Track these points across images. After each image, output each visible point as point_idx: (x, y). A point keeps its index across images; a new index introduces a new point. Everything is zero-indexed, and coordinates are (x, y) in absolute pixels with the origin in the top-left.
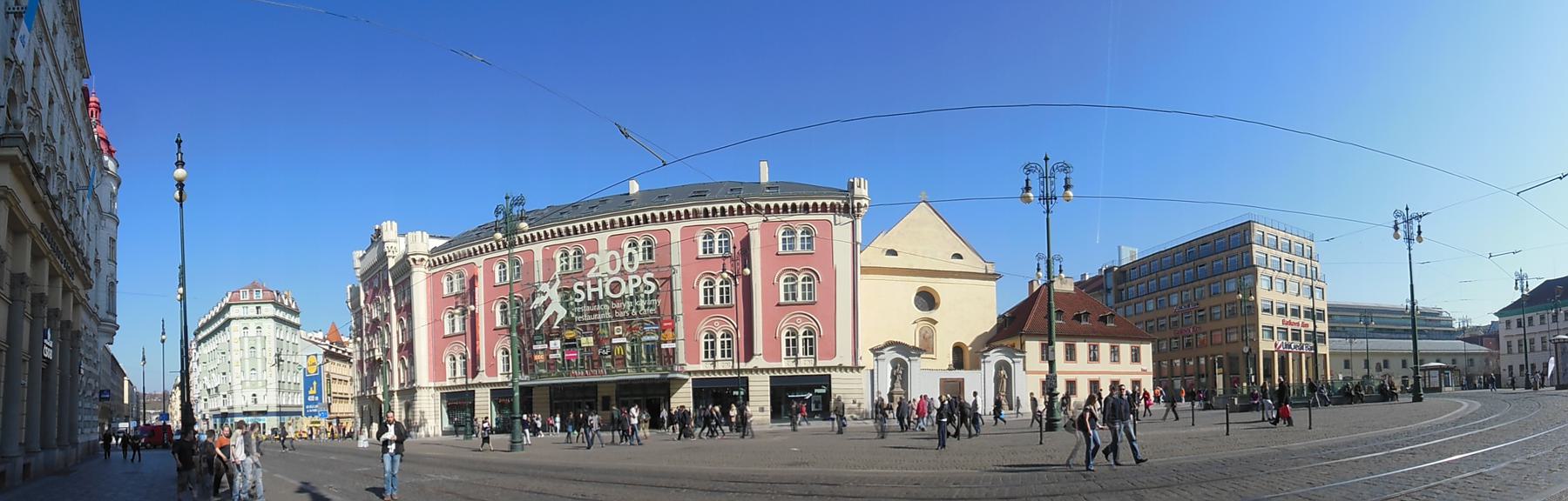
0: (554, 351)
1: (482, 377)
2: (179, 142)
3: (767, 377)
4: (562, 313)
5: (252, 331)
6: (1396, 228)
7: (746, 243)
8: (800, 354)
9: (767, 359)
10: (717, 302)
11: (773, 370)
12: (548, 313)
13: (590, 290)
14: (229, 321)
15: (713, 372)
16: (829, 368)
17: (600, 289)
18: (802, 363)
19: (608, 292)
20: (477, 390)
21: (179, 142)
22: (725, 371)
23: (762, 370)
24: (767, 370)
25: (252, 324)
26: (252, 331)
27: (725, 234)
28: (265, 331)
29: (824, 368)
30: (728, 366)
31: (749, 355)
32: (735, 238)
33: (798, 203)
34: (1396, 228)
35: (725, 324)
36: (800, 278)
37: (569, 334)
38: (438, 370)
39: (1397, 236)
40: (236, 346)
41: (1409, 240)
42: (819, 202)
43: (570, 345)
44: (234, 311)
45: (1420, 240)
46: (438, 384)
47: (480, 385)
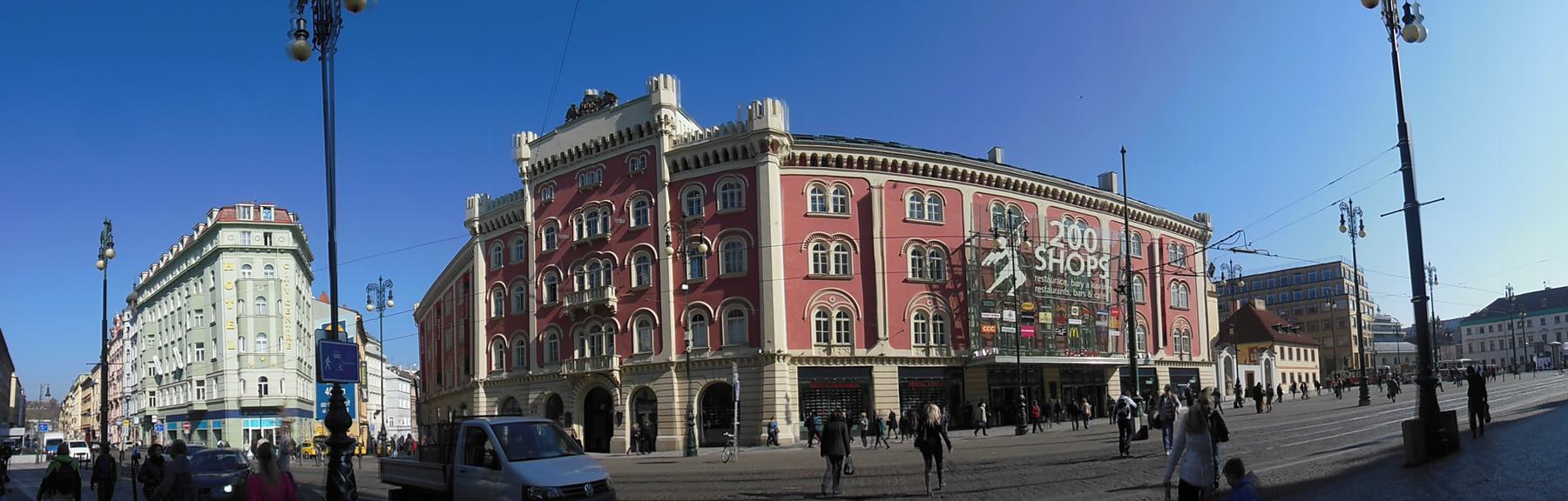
0: (1009, 324)
1: (884, 348)
2: (1123, 151)
3: (895, 367)
4: (1021, 279)
5: (258, 271)
6: (1343, 222)
7: (865, 205)
8: (834, 341)
9: (895, 345)
10: (832, 272)
11: (902, 359)
12: (1005, 274)
13: (1052, 260)
14: (217, 253)
15: (828, 360)
16: (870, 359)
17: (1061, 262)
18: (836, 352)
19: (1068, 266)
20: (877, 368)
21: (1123, 151)
22: (842, 359)
23: (889, 360)
24: (895, 360)
25: (258, 260)
26: (258, 271)
27: (841, 190)
28: (279, 272)
29: (863, 359)
30: (845, 352)
31: (871, 339)
32: (855, 193)
33: (821, 154)
34: (1343, 222)
35: (841, 300)
36: (833, 245)
37: (1028, 306)
38: (797, 334)
39: (1343, 230)
40: (228, 296)
41: (1353, 234)
42: (856, 157)
43: (1026, 318)
44: (226, 238)
45: (1363, 235)
46: (796, 353)
47: (882, 359)
